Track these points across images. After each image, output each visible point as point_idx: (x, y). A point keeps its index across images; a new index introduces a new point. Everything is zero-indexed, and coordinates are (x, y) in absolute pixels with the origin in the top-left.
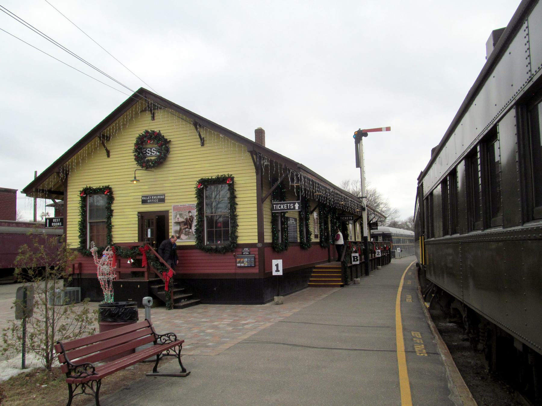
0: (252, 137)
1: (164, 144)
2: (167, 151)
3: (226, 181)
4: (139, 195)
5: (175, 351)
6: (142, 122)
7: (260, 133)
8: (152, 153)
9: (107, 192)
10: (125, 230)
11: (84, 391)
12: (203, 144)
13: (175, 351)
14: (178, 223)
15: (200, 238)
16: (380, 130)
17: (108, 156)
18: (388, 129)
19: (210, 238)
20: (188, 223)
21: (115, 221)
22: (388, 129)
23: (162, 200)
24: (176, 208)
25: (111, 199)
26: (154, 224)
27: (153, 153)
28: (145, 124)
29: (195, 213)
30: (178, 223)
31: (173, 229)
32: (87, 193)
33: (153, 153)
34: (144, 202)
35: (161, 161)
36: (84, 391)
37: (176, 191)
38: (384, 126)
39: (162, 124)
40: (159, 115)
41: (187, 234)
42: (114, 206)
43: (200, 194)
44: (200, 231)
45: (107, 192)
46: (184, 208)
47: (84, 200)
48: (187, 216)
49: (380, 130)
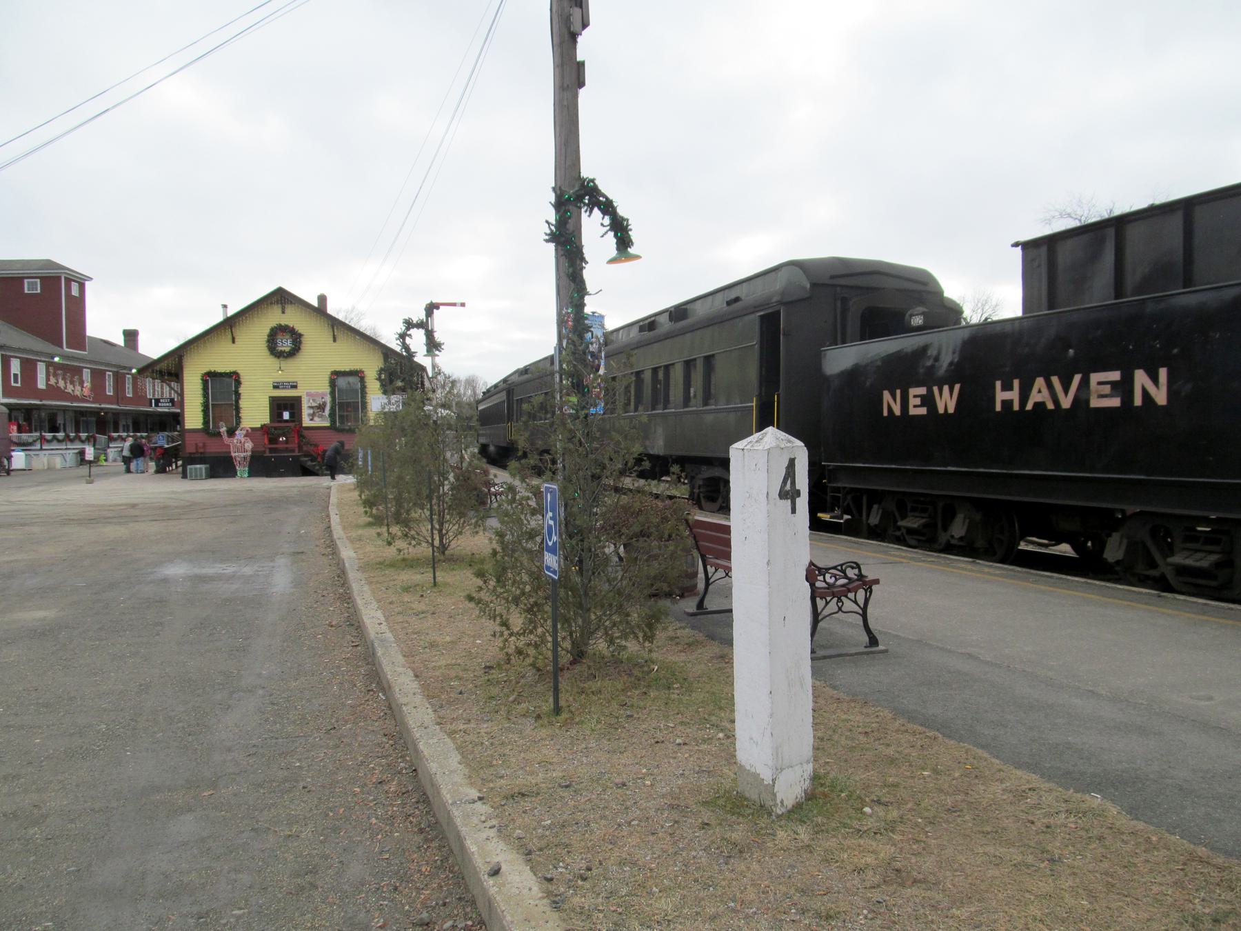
0: (315, 303)
1: (297, 338)
2: (300, 342)
3: (358, 374)
4: (270, 381)
5: (855, 602)
6: (282, 320)
7: (322, 299)
8: (285, 344)
9: (234, 378)
10: (255, 412)
11: (840, 609)
12: (335, 340)
13: (855, 602)
14: (311, 407)
15: (333, 422)
16: (454, 305)
17: (234, 342)
18: (463, 305)
19: (342, 422)
20: (321, 407)
21: (243, 403)
22: (463, 305)
23: (295, 387)
24: (308, 394)
25: (238, 383)
26: (284, 406)
27: (286, 344)
28: (274, 317)
29: (328, 399)
30: (311, 407)
31: (306, 412)
32: (211, 378)
33: (286, 344)
34: (276, 387)
35: (295, 351)
36: (840, 609)
37: (311, 377)
38: (459, 301)
39: (291, 318)
40: (290, 309)
41: (321, 416)
42: (241, 390)
43: (333, 384)
44: (332, 415)
45: (234, 378)
46: (317, 394)
47: (205, 383)
48: (320, 401)
49: (454, 305)
